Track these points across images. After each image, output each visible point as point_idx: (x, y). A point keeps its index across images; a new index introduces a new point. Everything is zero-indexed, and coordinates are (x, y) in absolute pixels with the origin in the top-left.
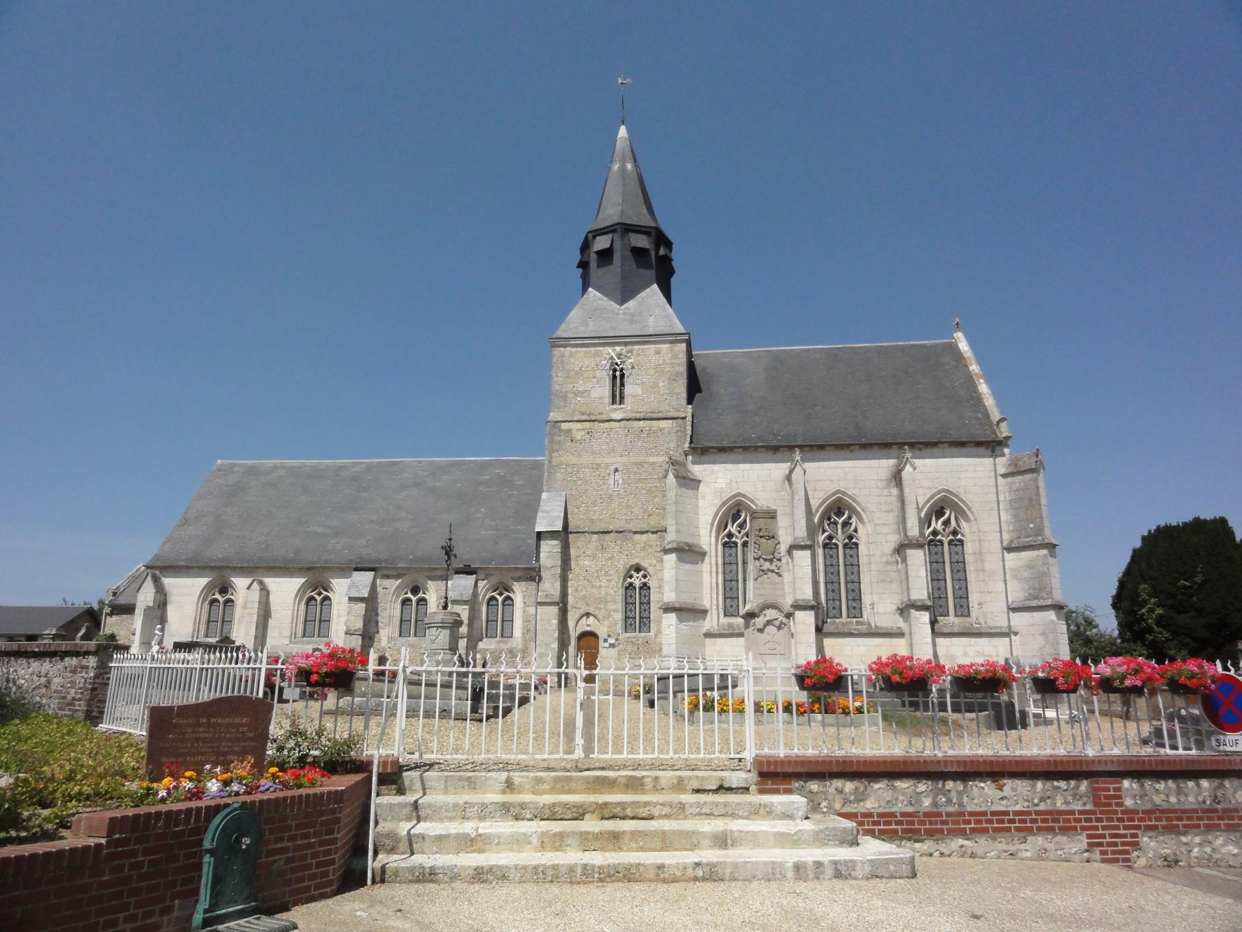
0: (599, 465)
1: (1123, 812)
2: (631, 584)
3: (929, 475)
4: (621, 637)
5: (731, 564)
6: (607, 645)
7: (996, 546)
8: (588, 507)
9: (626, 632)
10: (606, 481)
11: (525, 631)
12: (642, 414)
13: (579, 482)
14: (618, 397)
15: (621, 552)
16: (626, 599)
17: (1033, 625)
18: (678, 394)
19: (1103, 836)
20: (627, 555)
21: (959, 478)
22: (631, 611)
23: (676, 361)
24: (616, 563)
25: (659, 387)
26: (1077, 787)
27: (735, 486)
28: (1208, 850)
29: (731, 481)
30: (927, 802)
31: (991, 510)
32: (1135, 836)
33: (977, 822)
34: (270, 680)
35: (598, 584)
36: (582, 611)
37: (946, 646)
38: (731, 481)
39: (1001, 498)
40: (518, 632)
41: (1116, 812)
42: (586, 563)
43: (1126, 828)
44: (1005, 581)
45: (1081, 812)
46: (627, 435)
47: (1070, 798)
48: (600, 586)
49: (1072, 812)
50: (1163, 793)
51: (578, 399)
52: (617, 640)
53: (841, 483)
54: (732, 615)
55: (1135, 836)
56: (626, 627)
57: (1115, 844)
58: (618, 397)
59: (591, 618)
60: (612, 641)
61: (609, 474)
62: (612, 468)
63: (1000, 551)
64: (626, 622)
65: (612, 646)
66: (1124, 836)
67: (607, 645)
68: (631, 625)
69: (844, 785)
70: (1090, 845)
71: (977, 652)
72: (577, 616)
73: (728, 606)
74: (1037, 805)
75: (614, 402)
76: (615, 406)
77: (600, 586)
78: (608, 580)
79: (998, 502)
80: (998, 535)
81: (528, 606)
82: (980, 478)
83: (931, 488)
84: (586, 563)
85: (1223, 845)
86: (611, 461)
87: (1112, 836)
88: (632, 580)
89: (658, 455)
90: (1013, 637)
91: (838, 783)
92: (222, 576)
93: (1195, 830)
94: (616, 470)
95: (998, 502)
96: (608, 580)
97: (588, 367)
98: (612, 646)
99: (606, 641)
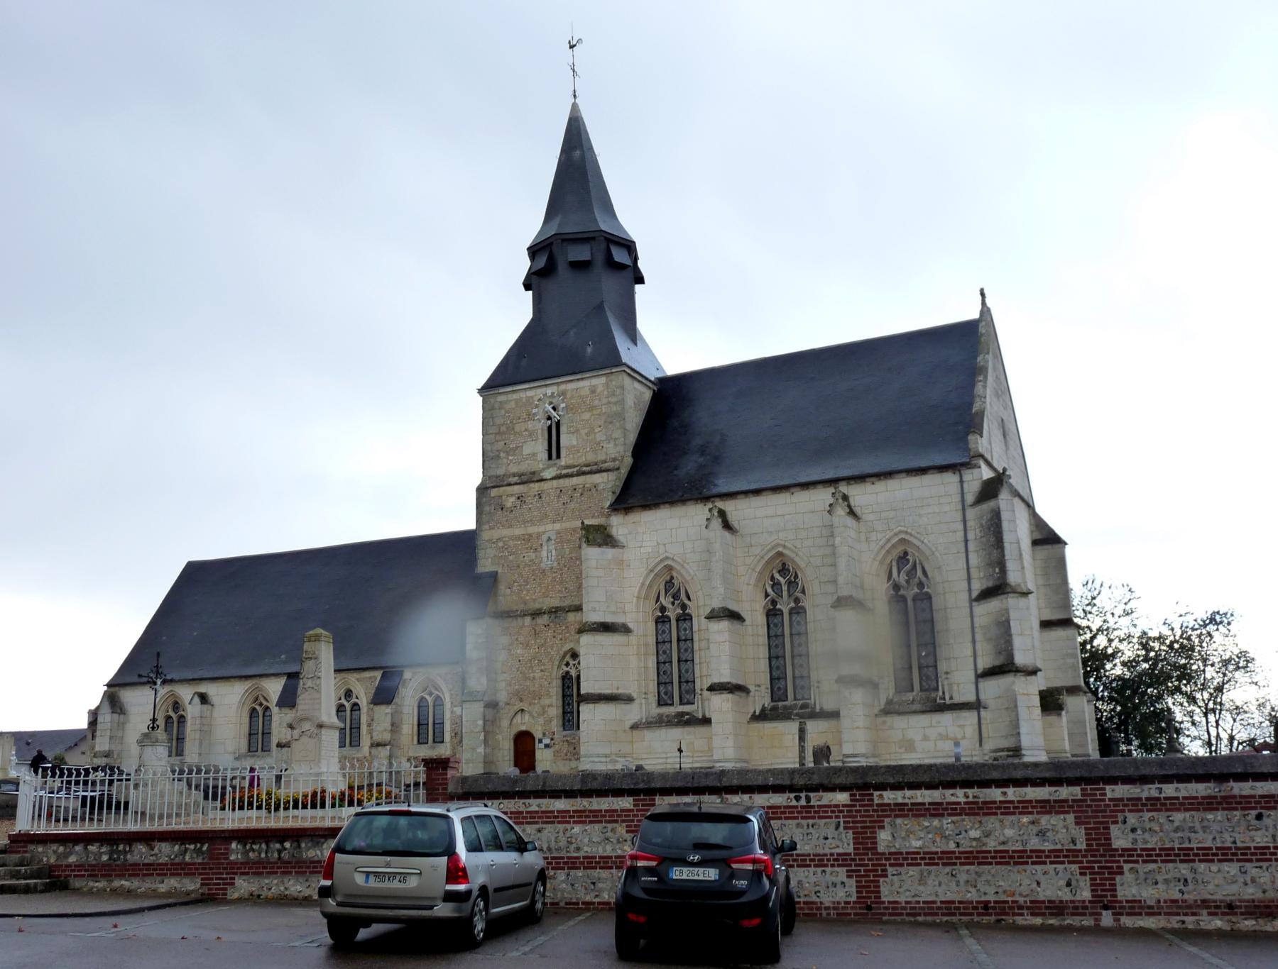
0: (530, 535)
1: (228, 864)
2: (567, 673)
3: (884, 515)
4: (556, 736)
5: (664, 642)
6: (542, 746)
7: (964, 597)
8: (520, 586)
9: (564, 729)
10: (538, 554)
11: (453, 735)
12: (575, 469)
13: (511, 558)
14: (554, 450)
15: (554, 637)
16: (563, 690)
17: (999, 697)
18: (615, 439)
19: (212, 879)
20: (561, 639)
21: (920, 516)
22: (569, 704)
23: (613, 400)
24: (549, 650)
25: (595, 433)
26: (201, 847)
27: (662, 550)
28: (282, 888)
29: (658, 544)
30: (105, 858)
31: (958, 552)
32: (232, 879)
33: (133, 870)
34: (1156, 778)
35: (532, 675)
36: (517, 708)
37: (903, 729)
38: (658, 544)
39: (971, 536)
40: (447, 737)
41: (223, 864)
42: (518, 651)
43: (227, 874)
44: (974, 642)
45: (199, 864)
46: (559, 497)
47: (195, 855)
48: (534, 678)
49: (194, 864)
50: (258, 851)
51: (511, 458)
52: (552, 739)
53: (780, 534)
54: (666, 704)
55: (232, 879)
56: (564, 724)
57: (219, 884)
58: (554, 450)
59: (527, 717)
60: (547, 741)
61: (542, 545)
62: (544, 537)
63: (968, 605)
64: (564, 718)
65: (547, 746)
66: (226, 879)
67: (542, 746)
68: (569, 721)
69: (58, 848)
70: (202, 884)
71: (940, 734)
72: (512, 713)
73: (662, 693)
74: (173, 859)
75: (550, 457)
76: (551, 462)
77: (534, 678)
78: (542, 671)
79: (966, 541)
80: (965, 584)
81: (455, 706)
82: (946, 512)
83: (884, 531)
84: (518, 651)
85: (293, 885)
86: (541, 529)
87: (217, 879)
88: (568, 669)
89: (593, 517)
90: (981, 710)
91: (54, 847)
92: (172, 691)
93: (275, 876)
94: (549, 539)
95: (966, 541)
96: (542, 671)
97: (519, 418)
98: (547, 746)
99: (540, 741)
